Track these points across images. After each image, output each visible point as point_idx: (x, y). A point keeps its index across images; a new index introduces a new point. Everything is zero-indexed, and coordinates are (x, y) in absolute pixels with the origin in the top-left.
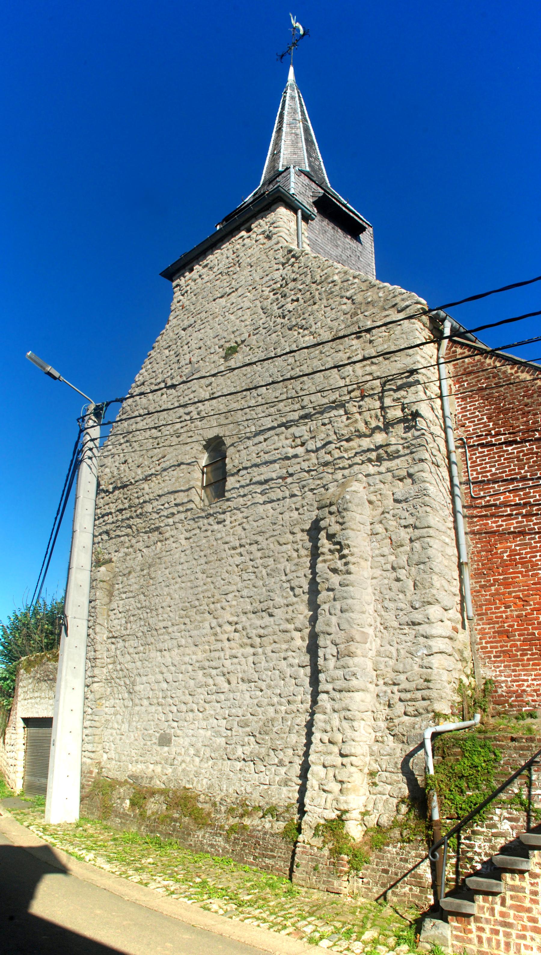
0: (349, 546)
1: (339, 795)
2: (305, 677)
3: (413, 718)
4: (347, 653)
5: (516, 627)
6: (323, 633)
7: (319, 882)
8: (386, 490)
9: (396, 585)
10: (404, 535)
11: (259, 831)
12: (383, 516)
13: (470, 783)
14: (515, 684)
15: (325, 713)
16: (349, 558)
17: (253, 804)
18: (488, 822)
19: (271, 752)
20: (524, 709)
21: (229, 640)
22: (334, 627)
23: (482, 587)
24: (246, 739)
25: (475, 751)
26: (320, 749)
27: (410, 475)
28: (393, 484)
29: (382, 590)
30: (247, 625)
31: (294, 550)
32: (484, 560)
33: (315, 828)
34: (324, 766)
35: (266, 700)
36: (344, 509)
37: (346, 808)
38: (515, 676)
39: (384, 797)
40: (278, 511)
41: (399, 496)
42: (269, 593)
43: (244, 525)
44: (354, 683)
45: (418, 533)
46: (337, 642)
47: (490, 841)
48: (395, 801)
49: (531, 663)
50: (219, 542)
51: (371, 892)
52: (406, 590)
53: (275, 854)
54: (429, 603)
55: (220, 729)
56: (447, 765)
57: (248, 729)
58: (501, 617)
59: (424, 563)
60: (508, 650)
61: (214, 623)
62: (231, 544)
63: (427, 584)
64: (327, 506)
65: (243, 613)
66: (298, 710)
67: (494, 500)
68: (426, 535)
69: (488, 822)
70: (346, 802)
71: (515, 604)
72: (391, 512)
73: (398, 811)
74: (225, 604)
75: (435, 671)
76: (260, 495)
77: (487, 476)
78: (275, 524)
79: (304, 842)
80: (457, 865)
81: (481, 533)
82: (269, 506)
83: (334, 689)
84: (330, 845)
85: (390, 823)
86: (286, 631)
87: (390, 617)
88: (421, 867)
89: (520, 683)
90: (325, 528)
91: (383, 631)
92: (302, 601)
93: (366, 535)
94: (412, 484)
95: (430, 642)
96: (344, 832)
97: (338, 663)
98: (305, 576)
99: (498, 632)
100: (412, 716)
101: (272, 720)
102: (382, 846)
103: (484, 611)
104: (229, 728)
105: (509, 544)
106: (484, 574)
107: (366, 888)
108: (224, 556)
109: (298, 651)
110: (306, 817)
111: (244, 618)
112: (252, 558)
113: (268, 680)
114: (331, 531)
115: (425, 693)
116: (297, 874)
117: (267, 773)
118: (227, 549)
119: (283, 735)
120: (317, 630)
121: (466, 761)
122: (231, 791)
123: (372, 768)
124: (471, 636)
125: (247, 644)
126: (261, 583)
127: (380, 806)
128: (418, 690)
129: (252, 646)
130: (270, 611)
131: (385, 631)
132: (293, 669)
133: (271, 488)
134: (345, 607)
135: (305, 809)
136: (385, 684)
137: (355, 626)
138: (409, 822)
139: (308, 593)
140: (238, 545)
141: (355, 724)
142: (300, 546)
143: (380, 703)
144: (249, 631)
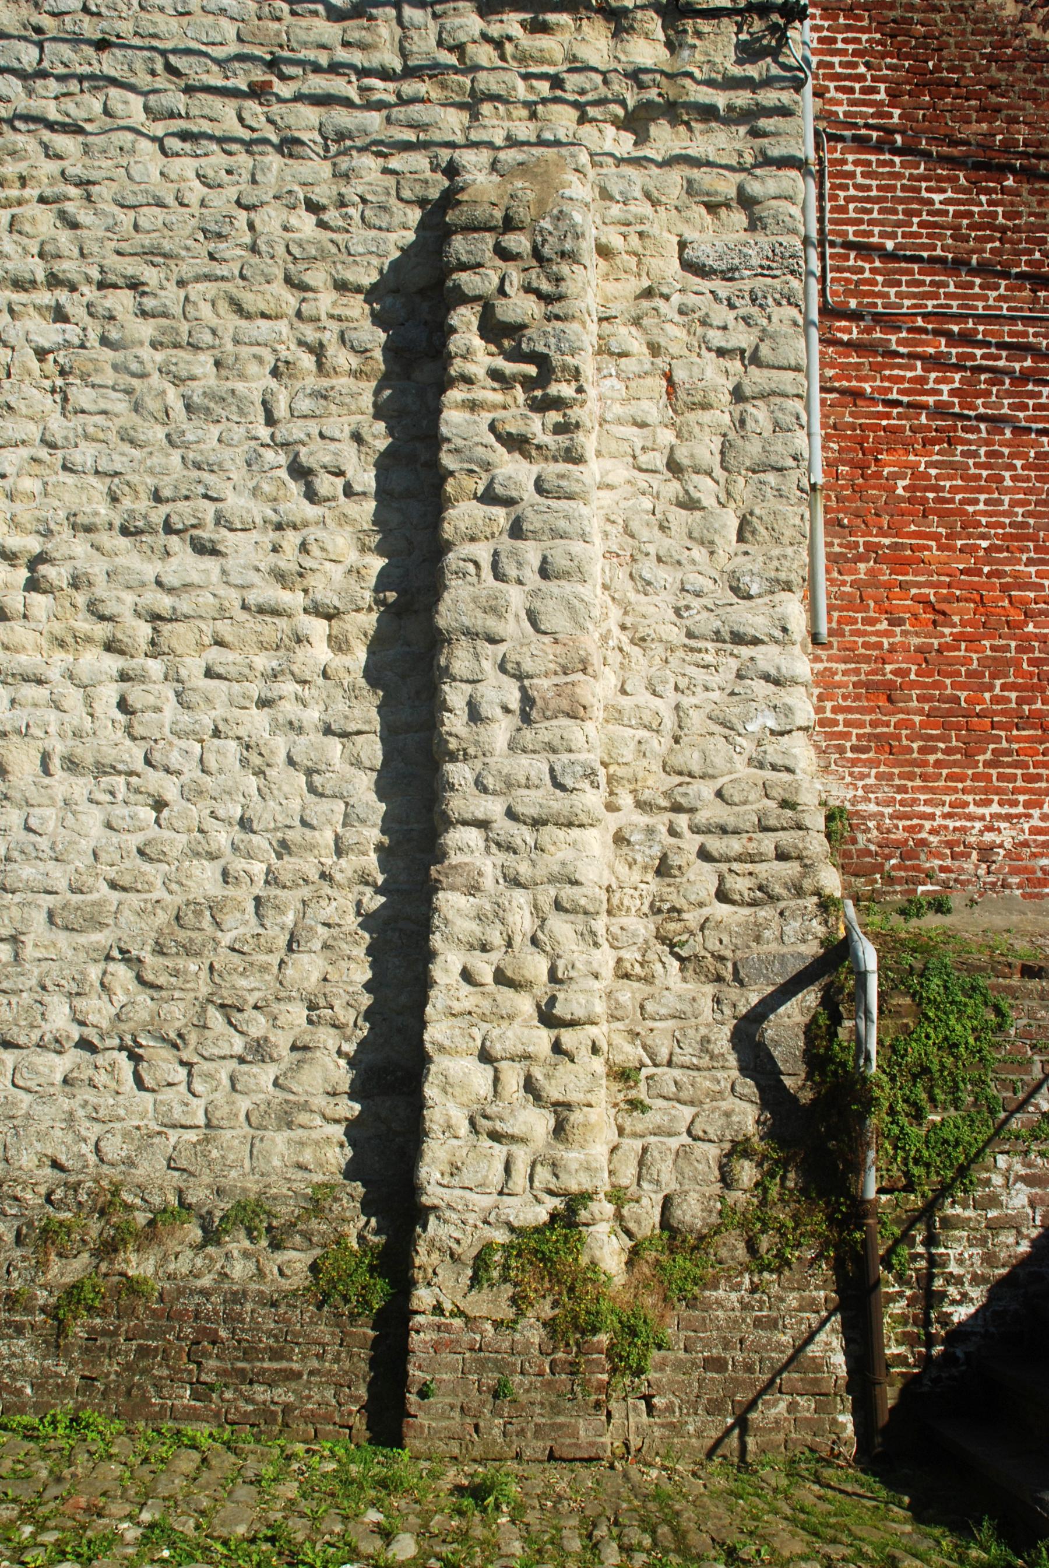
0: (576, 374)
3: (746, 911)
5: (913, 677)
6: (471, 634)
7: (521, 1433)
9: (679, 517)
10: (715, 376)
11: (205, 1293)
12: (645, 304)
13: (937, 1091)
14: (901, 824)
15: (473, 889)
16: (575, 414)
19: (215, 1018)
20: (921, 888)
26: (467, 1005)
27: (746, 201)
29: (635, 526)
30: (97, 568)
33: (477, 1257)
34: (485, 1057)
35: (183, 838)
36: (563, 254)
38: (902, 803)
39: (674, 1143)
41: (704, 252)
42: (195, 474)
43: (70, 207)
45: (758, 378)
46: (528, 666)
47: (983, 1241)
48: (713, 1151)
49: (945, 772)
52: (717, 539)
53: (296, 1366)
57: (100, 938)
58: (879, 646)
60: (891, 736)
65: (74, 527)
66: (323, 876)
69: (979, 1193)
71: (915, 616)
72: (676, 299)
79: (438, 1309)
83: (511, 814)
85: (714, 1219)
87: (657, 613)
89: (915, 822)
91: (627, 648)
92: (344, 519)
94: (752, 228)
96: (584, 1261)
97: (528, 735)
98: (357, 437)
99: (867, 685)
100: (742, 904)
101: (215, 908)
105: (912, 458)
106: (842, 526)
107: (662, 1426)
109: (320, 681)
111: (80, 547)
113: (191, 772)
115: (786, 838)
116: (426, 1419)
119: (262, 958)
125: (89, 640)
126: (159, 433)
127: (665, 1170)
129: (110, 646)
130: (204, 534)
131: (635, 651)
132: (302, 739)
134: (560, 562)
135: (425, 1200)
136: (642, 805)
142: (330, 337)
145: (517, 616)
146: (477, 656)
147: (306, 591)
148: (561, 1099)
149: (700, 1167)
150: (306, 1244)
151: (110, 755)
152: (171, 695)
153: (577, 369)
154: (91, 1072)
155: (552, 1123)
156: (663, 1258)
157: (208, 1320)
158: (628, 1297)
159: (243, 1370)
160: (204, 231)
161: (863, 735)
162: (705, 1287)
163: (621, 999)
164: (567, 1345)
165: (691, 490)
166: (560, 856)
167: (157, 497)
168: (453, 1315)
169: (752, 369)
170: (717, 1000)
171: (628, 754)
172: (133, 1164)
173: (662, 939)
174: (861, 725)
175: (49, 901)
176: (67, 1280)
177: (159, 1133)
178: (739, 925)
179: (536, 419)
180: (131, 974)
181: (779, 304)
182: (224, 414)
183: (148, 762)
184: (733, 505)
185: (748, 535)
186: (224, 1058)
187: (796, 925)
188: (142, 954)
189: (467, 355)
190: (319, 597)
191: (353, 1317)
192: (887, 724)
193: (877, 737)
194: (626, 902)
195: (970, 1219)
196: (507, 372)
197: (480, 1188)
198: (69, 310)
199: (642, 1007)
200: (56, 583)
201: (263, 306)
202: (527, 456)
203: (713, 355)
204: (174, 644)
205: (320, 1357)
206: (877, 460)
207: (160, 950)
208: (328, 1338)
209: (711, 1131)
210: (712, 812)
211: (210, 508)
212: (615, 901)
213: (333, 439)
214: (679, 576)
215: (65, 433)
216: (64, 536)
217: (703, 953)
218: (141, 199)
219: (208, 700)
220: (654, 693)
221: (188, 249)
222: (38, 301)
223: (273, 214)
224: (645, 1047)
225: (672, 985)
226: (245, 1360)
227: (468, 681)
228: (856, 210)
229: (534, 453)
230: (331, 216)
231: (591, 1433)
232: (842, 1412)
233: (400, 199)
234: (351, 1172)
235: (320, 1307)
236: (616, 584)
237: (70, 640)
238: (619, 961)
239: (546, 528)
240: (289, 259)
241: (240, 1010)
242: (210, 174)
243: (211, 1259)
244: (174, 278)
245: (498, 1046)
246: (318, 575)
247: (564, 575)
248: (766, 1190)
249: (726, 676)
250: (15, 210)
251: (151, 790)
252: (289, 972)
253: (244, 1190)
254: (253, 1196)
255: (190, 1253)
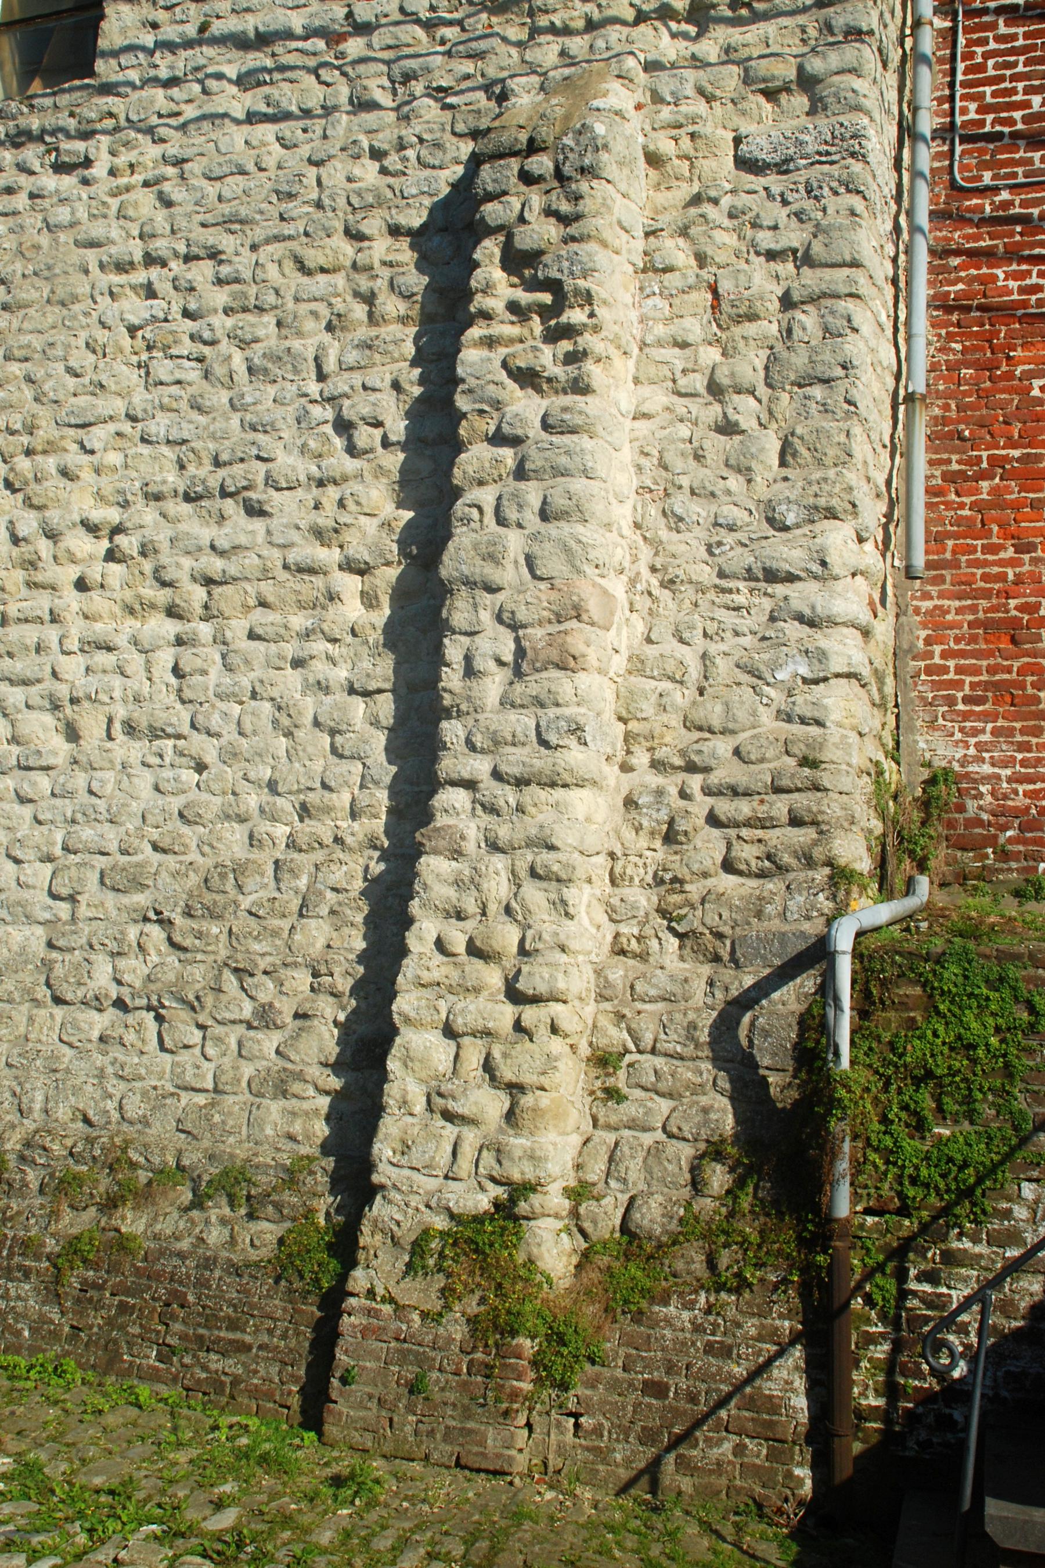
0: (588, 298)
1: (501, 1130)
2: (373, 730)
3: (753, 883)
4: (554, 655)
6: (470, 583)
7: (431, 1433)
8: (717, 126)
9: (716, 445)
10: (763, 282)
11: (181, 1255)
12: (693, 211)
13: (946, 1099)
15: (456, 854)
16: (587, 340)
17: (156, 1160)
18: (995, 1225)
19: (230, 982)
21: (81, 585)
22: (510, 567)
23: (950, 477)
24: (133, 933)
25: (971, 995)
26: (436, 975)
27: (807, 82)
28: (744, 105)
29: (669, 457)
30: (162, 537)
31: (357, 294)
32: (965, 394)
33: (415, 1243)
34: (449, 1032)
35: (218, 800)
36: (582, 170)
37: (530, 1176)
38: (1024, 763)
39: (647, 1139)
40: (305, 151)
41: (759, 148)
42: (251, 436)
43: (167, 187)
44: (574, 757)
46: (522, 615)
48: (687, 1151)
50: (63, 237)
51: (605, 1462)
52: (754, 465)
53: (248, 1339)
54: (831, 514)
55: (26, 894)
56: (878, 1038)
57: (141, 899)
58: (1002, 577)
59: (826, 381)
61: (28, 524)
62: (113, 250)
63: (831, 452)
64: (515, 154)
65: (147, 496)
66: (338, 840)
67: (1024, 204)
68: (844, 290)
69: (995, 1225)
70: (532, 1157)
72: (726, 201)
73: (697, 1184)
74: (74, 458)
75: (834, 733)
76: (234, 90)
77: (1011, 122)
78: (291, 196)
79: (371, 1293)
80: (891, 1366)
81: (968, 309)
82: (267, 131)
83: (497, 775)
84: (472, 1305)
85: (674, 1226)
86: (312, 571)
87: (688, 550)
88: (775, 1372)
90: (500, 228)
92: (380, 471)
93: (631, 269)
94: (811, 112)
95: (823, 640)
96: (520, 1258)
97: (519, 688)
98: (396, 386)
99: (985, 624)
100: (749, 875)
101: (239, 870)
102: (644, 1304)
103: (948, 555)
104: (65, 892)
106: (962, 439)
107: (587, 1449)
108: (83, 289)
109: (349, 639)
110: (379, 1208)
111: (148, 515)
112: (192, 306)
113: (229, 733)
114: (525, 239)
115: (802, 801)
116: (345, 1407)
117: (210, 1051)
118: (94, 267)
119: (275, 923)
120: (448, 568)
121: (941, 1029)
122: (63, 1112)
123: (603, 1042)
124: (897, 632)
125: (153, 606)
126: (223, 397)
127: (634, 1168)
128: (778, 790)
129: (172, 612)
132: (328, 700)
133: (282, 68)
134: (559, 501)
135: (376, 1178)
136: (656, 765)
137: (589, 570)
138: (739, 1225)
139: (404, 446)
140: (138, 257)
141: (571, 894)
142: (381, 285)
143: (638, 829)
144: (164, 559)
145: (516, 562)
146: (475, 606)
147: (341, 547)
148: (514, 1080)
149: (670, 1167)
150: (277, 1216)
151: (161, 718)
152: (218, 658)
153: (588, 292)
154: (122, 1030)
155: (507, 1105)
156: (616, 1264)
157: (181, 1283)
158: (567, 1302)
159: (202, 1336)
160: (277, 192)
161: (979, 684)
162: (652, 1301)
163: (611, 977)
164: (486, 1345)
165: (730, 411)
166: (541, 817)
167: (217, 463)
168: (383, 1300)
169: (805, 270)
170: (711, 983)
171: (648, 708)
172: (147, 1124)
173: (663, 912)
174: (975, 671)
175: (100, 862)
176: (74, 1231)
177: (172, 1094)
178: (741, 899)
179: (547, 350)
180: (163, 935)
181: (836, 193)
182: (279, 373)
183: (193, 726)
184: (775, 426)
185: (789, 458)
186: (233, 1022)
187: (800, 899)
188: (173, 915)
189: (487, 289)
190: (351, 552)
191: (305, 1294)
192: (1009, 670)
193: (996, 686)
194: (629, 871)
195: (980, 1256)
196: (523, 303)
197: (427, 1169)
198: (157, 286)
199: (632, 987)
200: (128, 552)
201: (322, 261)
202: (539, 390)
203: (762, 259)
204: (223, 606)
205: (270, 1332)
206: (1009, 358)
207: (188, 913)
208: (279, 1313)
209: (686, 1128)
210: (723, 774)
211: (262, 468)
212: (618, 870)
213: (374, 390)
214: (714, 508)
215: (144, 405)
216: (139, 506)
217: (701, 929)
218: (226, 170)
219: (247, 662)
220: (682, 641)
221: (261, 212)
222: (133, 281)
223: (339, 166)
224: (629, 1031)
225: (667, 963)
226: (206, 1327)
227: (467, 634)
228: (996, 67)
229: (545, 387)
230: (392, 161)
231: (499, 1444)
232: (800, 1464)
233: (454, 133)
234: (326, 1148)
235: (277, 1281)
236: (649, 522)
237: (137, 607)
238: (617, 935)
239: (547, 465)
240: (349, 209)
241: (252, 975)
242: (288, 134)
243: (193, 1222)
244: (248, 243)
245: (460, 1020)
246: (353, 530)
247: (563, 515)
248: (736, 1198)
249: (756, 620)
250: (124, 197)
251: (194, 753)
252: (297, 937)
253: (232, 1156)
254: (239, 1163)
255: (176, 1215)
